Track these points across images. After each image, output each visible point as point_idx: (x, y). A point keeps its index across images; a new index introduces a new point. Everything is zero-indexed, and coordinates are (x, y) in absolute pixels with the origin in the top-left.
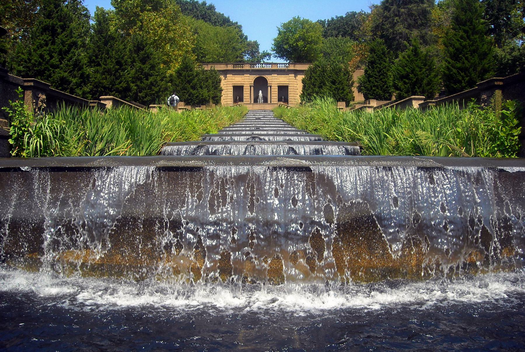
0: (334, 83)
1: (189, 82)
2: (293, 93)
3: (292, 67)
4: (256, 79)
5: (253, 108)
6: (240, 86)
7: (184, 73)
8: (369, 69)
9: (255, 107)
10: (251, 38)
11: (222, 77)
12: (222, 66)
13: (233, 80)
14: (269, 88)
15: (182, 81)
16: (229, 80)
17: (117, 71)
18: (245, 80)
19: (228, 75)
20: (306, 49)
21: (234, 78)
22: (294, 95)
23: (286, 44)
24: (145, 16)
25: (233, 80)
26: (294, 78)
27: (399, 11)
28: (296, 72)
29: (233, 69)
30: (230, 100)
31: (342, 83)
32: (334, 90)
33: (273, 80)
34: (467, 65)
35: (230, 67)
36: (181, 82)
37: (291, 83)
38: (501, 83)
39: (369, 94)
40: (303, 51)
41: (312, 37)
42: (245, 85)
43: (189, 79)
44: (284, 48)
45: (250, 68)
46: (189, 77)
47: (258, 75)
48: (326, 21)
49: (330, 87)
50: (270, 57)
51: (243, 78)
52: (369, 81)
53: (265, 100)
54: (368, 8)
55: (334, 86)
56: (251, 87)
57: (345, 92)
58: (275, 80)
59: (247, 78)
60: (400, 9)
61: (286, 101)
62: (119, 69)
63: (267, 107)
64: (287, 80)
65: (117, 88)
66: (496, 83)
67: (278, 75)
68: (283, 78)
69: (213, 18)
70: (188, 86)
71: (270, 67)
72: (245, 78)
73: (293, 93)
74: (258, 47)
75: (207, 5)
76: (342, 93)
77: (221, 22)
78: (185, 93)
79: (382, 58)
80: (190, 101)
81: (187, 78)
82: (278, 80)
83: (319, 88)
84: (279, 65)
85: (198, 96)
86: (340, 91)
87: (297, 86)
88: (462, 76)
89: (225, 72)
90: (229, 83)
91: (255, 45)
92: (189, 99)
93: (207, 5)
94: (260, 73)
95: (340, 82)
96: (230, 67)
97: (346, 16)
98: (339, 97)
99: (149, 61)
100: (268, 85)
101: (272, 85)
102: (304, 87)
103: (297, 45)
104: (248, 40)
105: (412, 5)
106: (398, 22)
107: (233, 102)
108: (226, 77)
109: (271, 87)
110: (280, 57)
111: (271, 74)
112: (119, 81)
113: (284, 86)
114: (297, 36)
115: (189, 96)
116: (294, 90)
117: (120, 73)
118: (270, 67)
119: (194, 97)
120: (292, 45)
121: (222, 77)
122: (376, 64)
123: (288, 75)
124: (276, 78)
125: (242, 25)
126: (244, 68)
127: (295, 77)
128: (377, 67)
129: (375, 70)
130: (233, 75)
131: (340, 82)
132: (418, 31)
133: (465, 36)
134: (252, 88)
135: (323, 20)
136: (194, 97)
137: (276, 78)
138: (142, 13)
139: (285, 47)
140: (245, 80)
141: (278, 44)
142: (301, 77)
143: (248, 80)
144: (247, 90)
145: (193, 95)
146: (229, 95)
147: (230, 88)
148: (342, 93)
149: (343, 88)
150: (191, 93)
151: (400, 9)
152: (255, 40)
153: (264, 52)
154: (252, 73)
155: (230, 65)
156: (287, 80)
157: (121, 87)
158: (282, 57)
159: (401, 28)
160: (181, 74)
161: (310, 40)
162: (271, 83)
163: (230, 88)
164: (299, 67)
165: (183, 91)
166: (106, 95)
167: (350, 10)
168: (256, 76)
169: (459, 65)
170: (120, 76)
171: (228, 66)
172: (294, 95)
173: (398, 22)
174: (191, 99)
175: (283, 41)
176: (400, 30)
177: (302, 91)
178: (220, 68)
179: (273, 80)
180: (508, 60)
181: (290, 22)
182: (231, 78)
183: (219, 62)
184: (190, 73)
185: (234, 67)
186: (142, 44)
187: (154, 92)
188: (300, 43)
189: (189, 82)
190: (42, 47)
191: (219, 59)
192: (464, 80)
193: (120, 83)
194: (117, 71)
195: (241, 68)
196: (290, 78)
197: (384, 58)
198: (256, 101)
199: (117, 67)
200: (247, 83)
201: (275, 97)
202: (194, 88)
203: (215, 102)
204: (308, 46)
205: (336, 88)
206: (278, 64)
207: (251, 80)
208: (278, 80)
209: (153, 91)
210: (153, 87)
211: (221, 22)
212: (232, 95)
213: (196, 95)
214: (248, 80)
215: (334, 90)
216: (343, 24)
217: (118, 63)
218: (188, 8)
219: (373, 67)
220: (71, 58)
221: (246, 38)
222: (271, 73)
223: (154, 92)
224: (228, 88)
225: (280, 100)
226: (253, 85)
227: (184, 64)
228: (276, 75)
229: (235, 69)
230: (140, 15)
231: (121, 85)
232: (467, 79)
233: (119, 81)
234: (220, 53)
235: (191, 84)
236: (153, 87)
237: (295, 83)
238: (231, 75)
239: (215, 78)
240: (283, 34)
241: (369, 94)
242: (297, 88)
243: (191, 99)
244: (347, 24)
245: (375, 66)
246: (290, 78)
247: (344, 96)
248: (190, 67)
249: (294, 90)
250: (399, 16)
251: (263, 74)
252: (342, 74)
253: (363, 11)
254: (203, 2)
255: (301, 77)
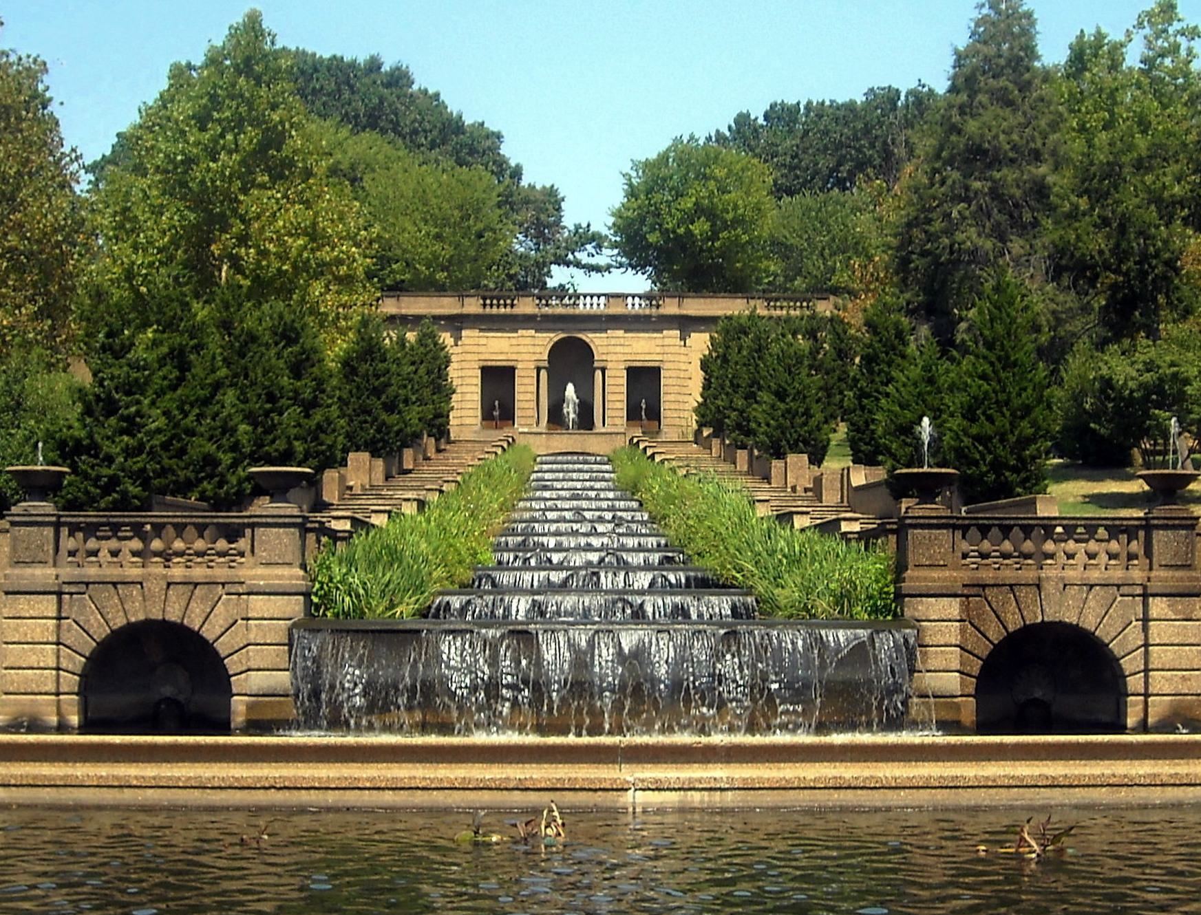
0: (781, 395)
1: (377, 392)
2: (676, 389)
3: (671, 308)
4: (556, 343)
5: (547, 448)
6: (504, 367)
7: (364, 368)
8: (863, 374)
9: (556, 444)
10: (534, 177)
11: (446, 338)
12: (446, 301)
13: (482, 349)
14: (598, 374)
15: (358, 388)
16: (467, 348)
17: (267, 414)
18: (521, 349)
19: (464, 333)
20: (717, 244)
21: (483, 341)
22: (681, 398)
23: (653, 230)
24: (250, 203)
25: (482, 349)
26: (678, 341)
27: (967, 188)
28: (686, 324)
29: (480, 311)
30: (471, 413)
31: (805, 397)
32: (783, 416)
33: (612, 349)
34: (989, 429)
35: (473, 306)
36: (354, 391)
37: (671, 357)
38: (895, 527)
39: (860, 439)
40: (710, 250)
41: (736, 207)
42: (520, 366)
43: (377, 383)
44: (650, 245)
45: (536, 311)
46: (377, 377)
47: (563, 330)
48: (802, 107)
49: (773, 406)
50: (599, 247)
51: (514, 342)
52: (863, 408)
53: (586, 420)
54: (950, 51)
55: (782, 406)
56: (538, 369)
57: (813, 422)
58: (618, 349)
59: (528, 341)
60: (969, 182)
61: (654, 414)
62: (271, 411)
63: (591, 443)
64: (658, 350)
65: (268, 454)
66: (888, 527)
67: (626, 331)
68: (642, 343)
69: (406, 122)
70: (375, 403)
71: (602, 306)
72: (521, 341)
73: (676, 389)
74: (559, 209)
75: (386, 68)
76: (805, 424)
77: (435, 133)
78: (366, 422)
79: (894, 348)
80: (380, 444)
81: (372, 380)
82: (627, 350)
83: (746, 399)
84: (630, 299)
85: (401, 430)
86: (798, 421)
87: (690, 367)
88: (979, 452)
89: (457, 323)
90: (469, 357)
91: (551, 200)
92: (379, 441)
93: (386, 68)
94: (571, 326)
95: (799, 392)
96: (473, 306)
97: (868, 102)
98: (795, 436)
99: (310, 370)
100: (596, 365)
101: (609, 365)
102: (707, 386)
103: (689, 232)
104: (524, 183)
105: (1005, 171)
106: (964, 218)
107: (480, 418)
108: (458, 338)
109: (603, 370)
110: (633, 267)
111: (605, 331)
112: (271, 437)
113: (648, 368)
114: (688, 203)
115: (379, 431)
116: (679, 382)
117: (272, 420)
118: (602, 306)
119: (392, 435)
120: (674, 232)
121: (446, 338)
122: (878, 364)
123: (660, 331)
124: (622, 341)
125: (504, 133)
126: (516, 311)
127: (683, 338)
128: (881, 371)
129: (877, 379)
130: (481, 330)
131: (799, 392)
132: (1021, 242)
133: (989, 370)
134: (543, 374)
135: (790, 101)
136: (392, 435)
137: (622, 341)
138: (245, 195)
139: (652, 238)
140: (521, 349)
141: (630, 225)
142: (700, 342)
143: (531, 349)
144: (526, 381)
145: (389, 427)
146: (468, 397)
147: (470, 373)
148: (805, 424)
149: (808, 409)
150: (384, 423)
151: (969, 182)
152: (548, 186)
153: (578, 227)
154: (544, 326)
155: (473, 300)
156: (658, 350)
157: (276, 450)
158: (638, 265)
159: (970, 236)
160: (354, 371)
161: (730, 216)
162: (604, 357)
163: (470, 373)
164: (695, 307)
165: (362, 418)
166: (853, 727)
167: (881, 80)
168: (553, 337)
169: (974, 430)
170: (274, 427)
171: (467, 300)
172: (681, 398)
173: (964, 218)
174: (382, 440)
175: (642, 221)
176: (969, 243)
177: (702, 396)
178: (442, 307)
179: (612, 349)
180: (1132, 391)
181: (663, 158)
182: (476, 341)
183: (440, 289)
184: (380, 365)
185: (484, 305)
186: (294, 329)
187: (324, 447)
188: (700, 227)
189: (377, 392)
190: (165, 394)
191: (432, 274)
192: (984, 460)
193: (273, 442)
194: (267, 414)
195: (508, 310)
196: (667, 341)
197: (901, 347)
198: (556, 418)
199: (268, 406)
200: (526, 357)
201: (619, 405)
202: (390, 408)
203: (434, 431)
204: (724, 234)
205: (788, 411)
206: (627, 296)
207: (538, 349)
208: (627, 350)
209: (321, 444)
210: (322, 436)
211: (435, 133)
212: (478, 397)
213: (396, 428)
214: (531, 349)
215: (783, 416)
216: (855, 135)
217: (271, 398)
218: (322, 88)
219: (871, 372)
220: (217, 414)
221: (517, 173)
222: (604, 326)
223: (324, 447)
224: (463, 373)
225: (633, 414)
226: (546, 364)
227: (363, 339)
228: (620, 333)
229: (488, 310)
230: (241, 202)
231: (274, 446)
232: (989, 458)
233: (271, 437)
234: (436, 257)
235: (383, 397)
236: (322, 436)
237: (683, 358)
238: (476, 333)
239: (435, 358)
240: (642, 197)
241: (860, 439)
242: (687, 375)
243: (382, 440)
244: (867, 130)
245: (876, 369)
246: (667, 341)
247: (810, 433)
248: (379, 349)
249: (679, 382)
250: (968, 200)
251: (580, 331)
252: (804, 371)
253: (924, 86)
254: (372, 57)
255: (700, 342)
